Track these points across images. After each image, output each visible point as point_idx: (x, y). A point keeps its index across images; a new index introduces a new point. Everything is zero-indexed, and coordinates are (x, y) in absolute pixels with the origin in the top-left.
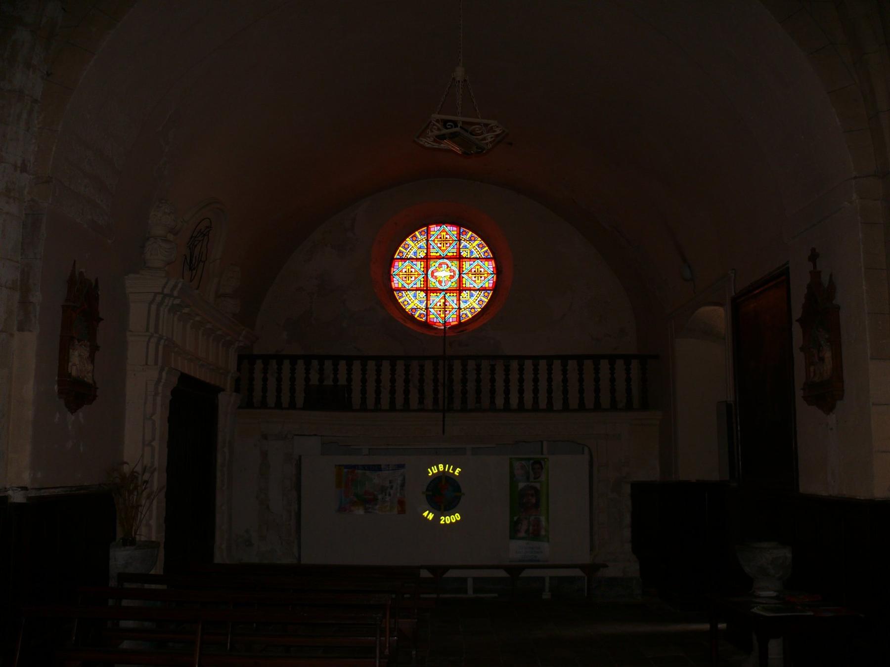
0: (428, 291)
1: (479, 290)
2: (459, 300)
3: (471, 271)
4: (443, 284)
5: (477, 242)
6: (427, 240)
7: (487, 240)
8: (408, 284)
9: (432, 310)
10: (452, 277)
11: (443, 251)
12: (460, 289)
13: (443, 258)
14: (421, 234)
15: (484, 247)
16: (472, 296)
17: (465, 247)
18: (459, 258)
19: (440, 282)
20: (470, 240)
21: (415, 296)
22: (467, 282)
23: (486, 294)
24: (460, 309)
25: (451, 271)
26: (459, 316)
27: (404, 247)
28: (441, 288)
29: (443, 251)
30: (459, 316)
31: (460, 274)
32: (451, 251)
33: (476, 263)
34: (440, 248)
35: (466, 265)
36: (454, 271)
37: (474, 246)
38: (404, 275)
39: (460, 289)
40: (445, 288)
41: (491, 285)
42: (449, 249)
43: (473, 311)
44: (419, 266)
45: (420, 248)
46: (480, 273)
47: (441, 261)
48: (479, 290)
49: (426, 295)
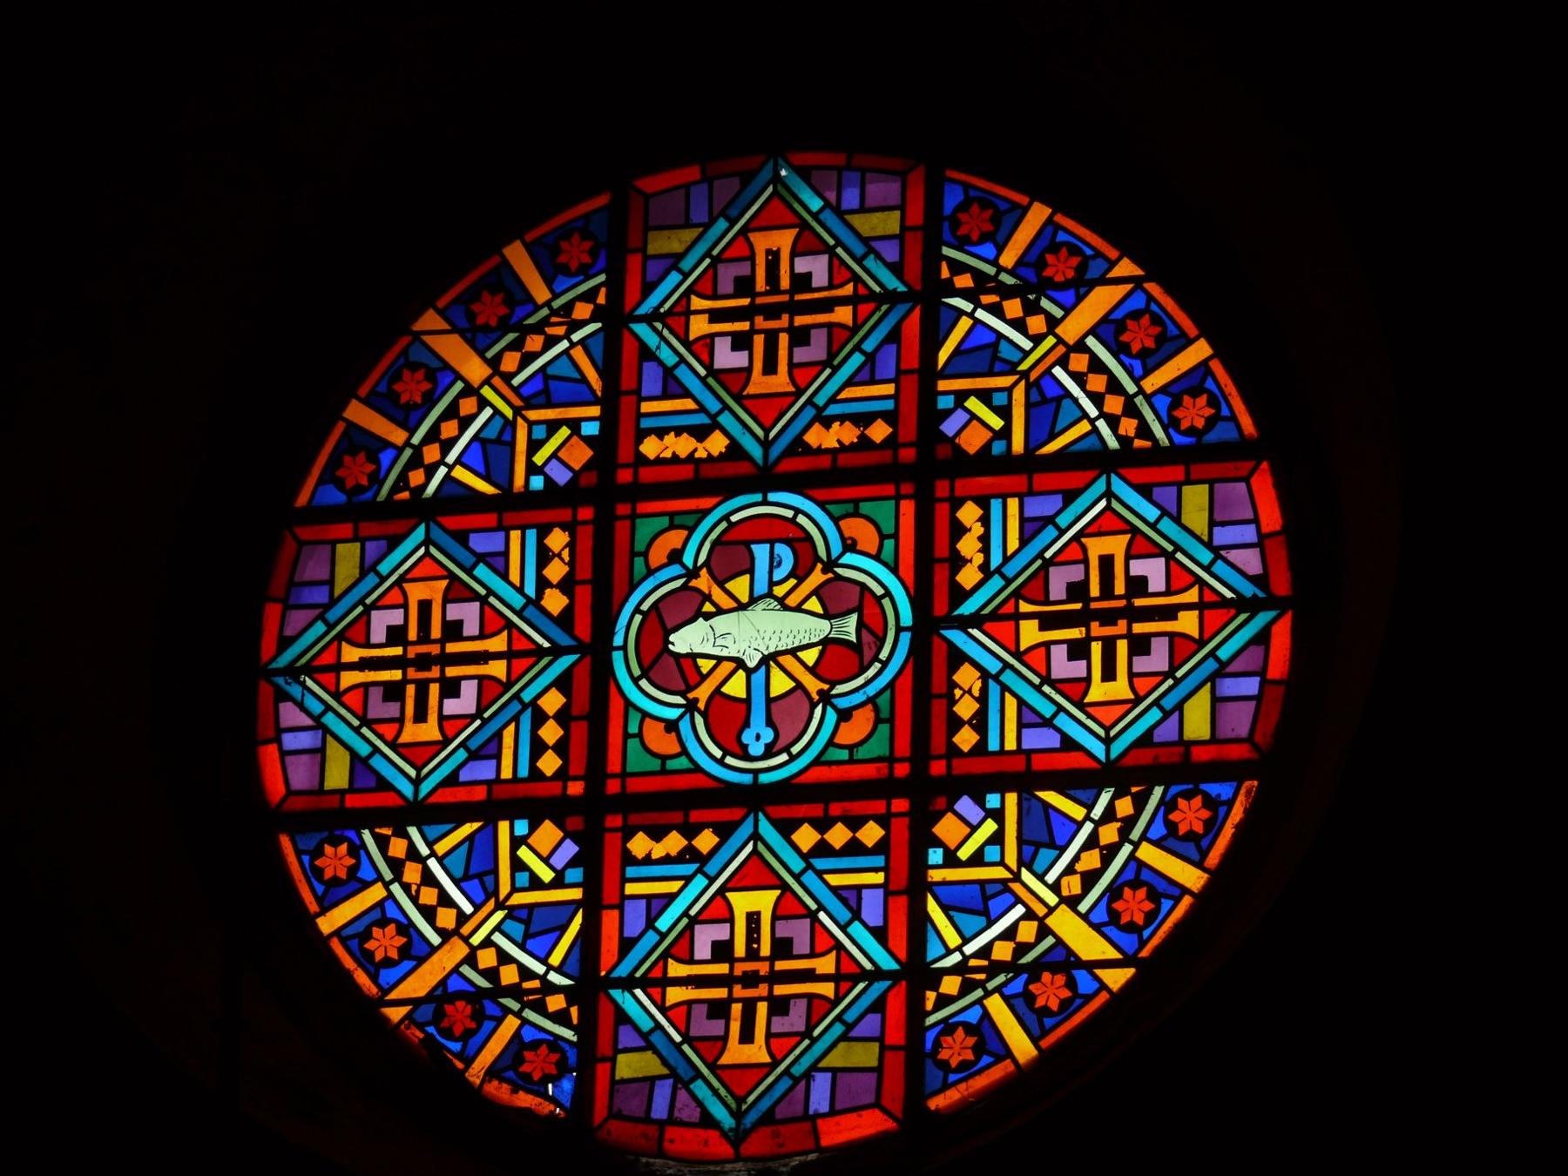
0: (602, 804)
1: (1120, 775)
2: (911, 887)
3: (1036, 587)
4: (757, 736)
5: (1100, 301)
6: (615, 318)
7: (1201, 272)
8: (418, 754)
9: (638, 1005)
10: (839, 659)
11: (766, 408)
12: (917, 776)
13: (765, 480)
14: (985, 1035)
15: (356, 936)
16: (1042, 835)
17: (985, 355)
18: (921, 471)
19: (727, 719)
20: (1033, 282)
21: (478, 873)
22: (1000, 697)
23: (1191, 815)
24: (918, 973)
25: (838, 597)
26: (915, 1055)
27: (1161, 889)
28: (734, 772)
29: (766, 408)
30: (915, 1055)
31: (926, 627)
32: (849, 406)
33: (1089, 505)
34: (734, 381)
35: (989, 535)
36: (865, 602)
37: (1066, 343)
38: (398, 668)
39: (917, 776)
40: (777, 770)
41: (1240, 721)
42: (827, 386)
43: (1050, 992)
44: (529, 569)
45: (544, 391)
46: (1132, 604)
47: (745, 507)
48: (1120, 775)
49: (932, 417)
